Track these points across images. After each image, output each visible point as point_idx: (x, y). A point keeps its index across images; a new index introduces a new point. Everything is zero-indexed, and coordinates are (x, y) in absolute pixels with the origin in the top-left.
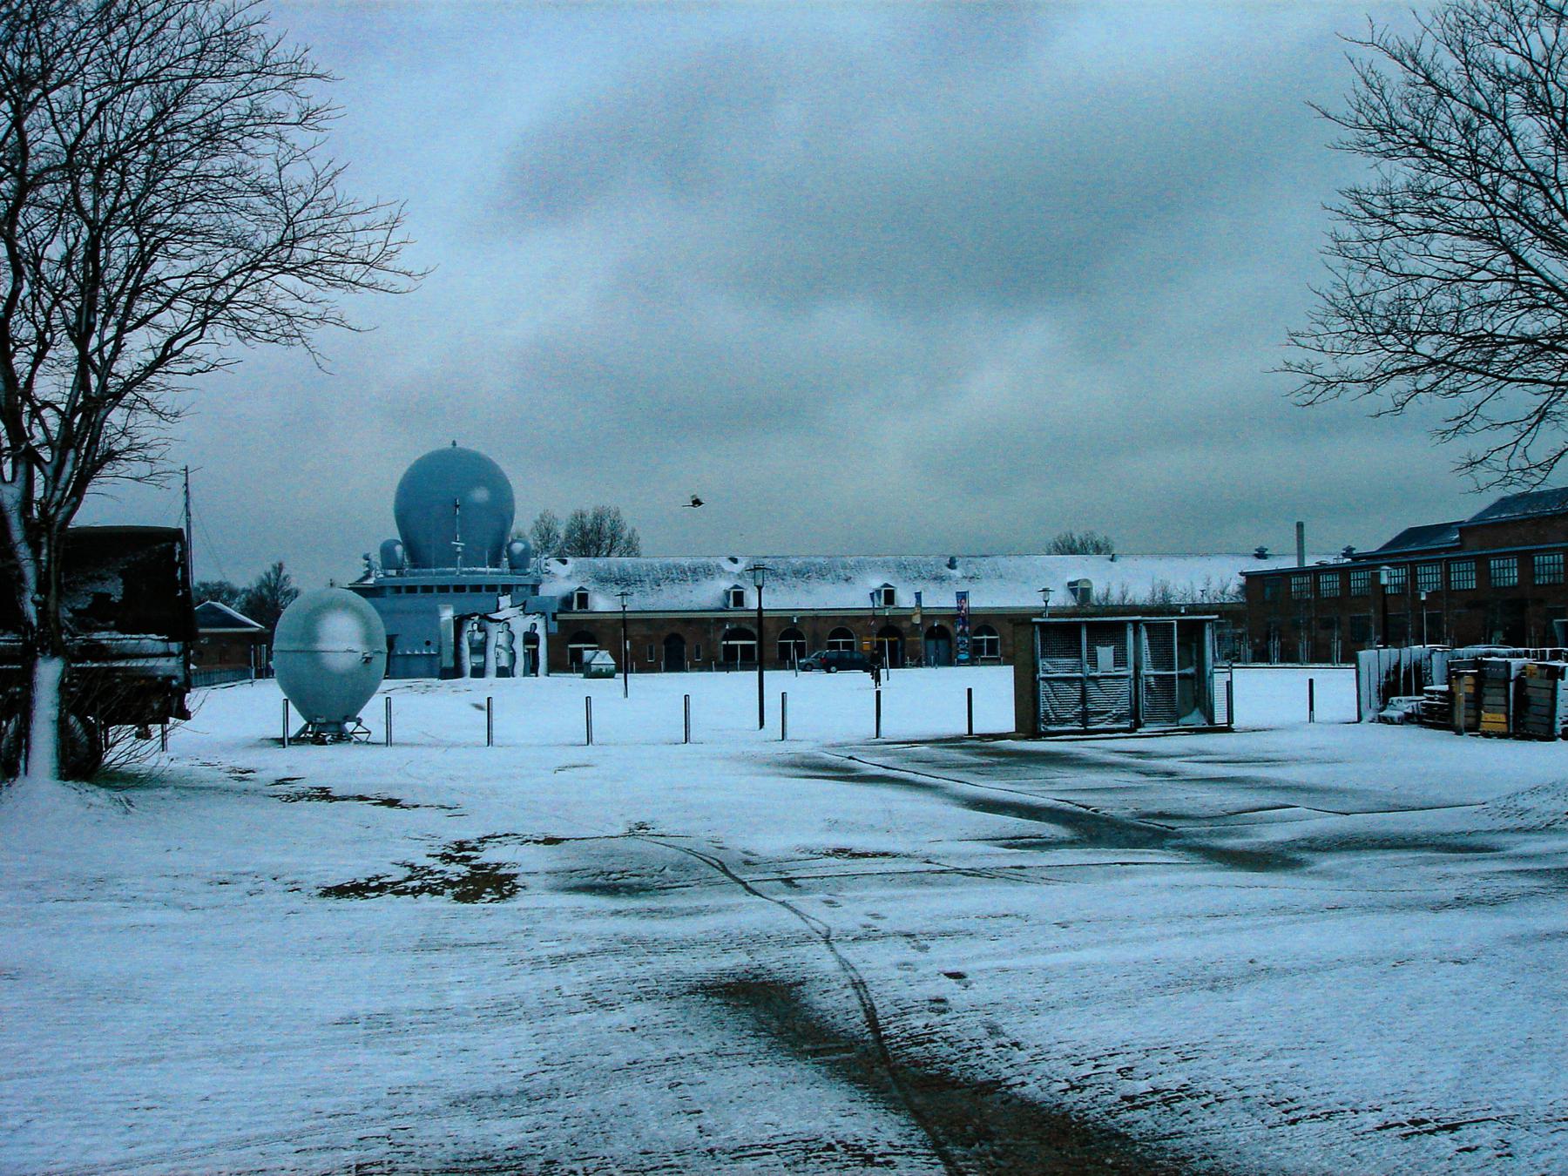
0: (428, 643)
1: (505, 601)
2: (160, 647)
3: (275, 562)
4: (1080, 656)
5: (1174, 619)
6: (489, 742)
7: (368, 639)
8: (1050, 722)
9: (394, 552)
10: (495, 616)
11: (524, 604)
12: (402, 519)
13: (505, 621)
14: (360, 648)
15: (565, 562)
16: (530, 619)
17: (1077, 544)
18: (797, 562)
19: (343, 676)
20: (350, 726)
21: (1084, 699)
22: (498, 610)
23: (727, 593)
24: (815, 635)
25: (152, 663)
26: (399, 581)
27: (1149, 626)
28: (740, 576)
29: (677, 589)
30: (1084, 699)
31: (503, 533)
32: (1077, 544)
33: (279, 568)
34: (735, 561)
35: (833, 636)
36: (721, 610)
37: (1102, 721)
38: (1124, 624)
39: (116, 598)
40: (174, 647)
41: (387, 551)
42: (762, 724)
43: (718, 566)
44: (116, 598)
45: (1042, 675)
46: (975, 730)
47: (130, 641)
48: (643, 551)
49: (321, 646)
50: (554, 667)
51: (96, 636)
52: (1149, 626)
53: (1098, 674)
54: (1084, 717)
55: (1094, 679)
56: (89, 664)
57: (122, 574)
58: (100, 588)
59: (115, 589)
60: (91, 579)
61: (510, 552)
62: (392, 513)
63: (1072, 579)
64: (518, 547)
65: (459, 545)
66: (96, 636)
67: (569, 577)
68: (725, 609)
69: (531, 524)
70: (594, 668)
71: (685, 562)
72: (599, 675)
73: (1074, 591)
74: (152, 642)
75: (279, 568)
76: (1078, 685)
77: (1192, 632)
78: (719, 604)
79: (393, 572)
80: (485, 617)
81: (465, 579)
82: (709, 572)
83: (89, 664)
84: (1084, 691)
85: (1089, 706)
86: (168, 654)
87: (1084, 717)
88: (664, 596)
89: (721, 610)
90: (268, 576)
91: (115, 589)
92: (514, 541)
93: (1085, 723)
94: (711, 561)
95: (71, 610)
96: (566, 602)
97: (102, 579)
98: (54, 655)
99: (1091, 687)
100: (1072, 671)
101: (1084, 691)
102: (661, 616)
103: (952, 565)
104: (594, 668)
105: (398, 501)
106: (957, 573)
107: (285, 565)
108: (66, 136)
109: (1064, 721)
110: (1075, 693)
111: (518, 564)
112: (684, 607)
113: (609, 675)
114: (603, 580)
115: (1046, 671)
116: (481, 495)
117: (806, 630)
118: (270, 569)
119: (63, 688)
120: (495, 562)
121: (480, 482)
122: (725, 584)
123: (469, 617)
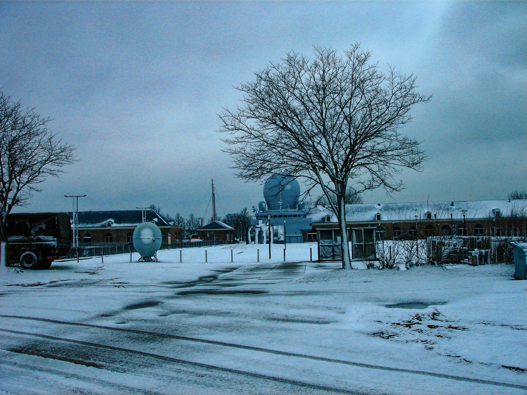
1: (260, 222)
2: (52, 239)
5: (363, 228)
6: (181, 262)
7: (154, 235)
8: (323, 258)
12: (266, 197)
13: (261, 228)
14: (151, 237)
17: (519, 195)
18: (400, 205)
19: (147, 244)
20: (153, 258)
21: (333, 251)
23: (375, 215)
25: (51, 242)
27: (356, 231)
28: (380, 210)
30: (333, 251)
31: (298, 197)
32: (519, 195)
34: (379, 205)
35: (410, 229)
36: (373, 221)
38: (332, 230)
39: (44, 228)
40: (55, 239)
41: (260, 205)
43: (374, 207)
44: (44, 228)
47: (46, 238)
48: (364, 202)
49: (142, 237)
51: (39, 237)
52: (356, 231)
54: (333, 256)
56: (38, 243)
57: (45, 223)
58: (41, 226)
59: (44, 226)
60: (39, 224)
63: (493, 208)
65: (281, 203)
66: (39, 237)
68: (375, 220)
73: (494, 212)
74: (51, 238)
77: (369, 232)
78: (372, 219)
80: (254, 226)
82: (371, 209)
83: (38, 243)
84: (333, 249)
85: (335, 253)
86: (54, 241)
88: (355, 217)
89: (373, 221)
90: (242, 212)
91: (44, 226)
93: (333, 258)
96: (323, 219)
97: (41, 224)
98: (4, 241)
99: (335, 248)
101: (333, 249)
102: (350, 223)
103: (452, 205)
106: (454, 207)
109: (328, 257)
110: (330, 250)
111: (301, 207)
118: (242, 210)
119: (6, 248)
122: (375, 212)
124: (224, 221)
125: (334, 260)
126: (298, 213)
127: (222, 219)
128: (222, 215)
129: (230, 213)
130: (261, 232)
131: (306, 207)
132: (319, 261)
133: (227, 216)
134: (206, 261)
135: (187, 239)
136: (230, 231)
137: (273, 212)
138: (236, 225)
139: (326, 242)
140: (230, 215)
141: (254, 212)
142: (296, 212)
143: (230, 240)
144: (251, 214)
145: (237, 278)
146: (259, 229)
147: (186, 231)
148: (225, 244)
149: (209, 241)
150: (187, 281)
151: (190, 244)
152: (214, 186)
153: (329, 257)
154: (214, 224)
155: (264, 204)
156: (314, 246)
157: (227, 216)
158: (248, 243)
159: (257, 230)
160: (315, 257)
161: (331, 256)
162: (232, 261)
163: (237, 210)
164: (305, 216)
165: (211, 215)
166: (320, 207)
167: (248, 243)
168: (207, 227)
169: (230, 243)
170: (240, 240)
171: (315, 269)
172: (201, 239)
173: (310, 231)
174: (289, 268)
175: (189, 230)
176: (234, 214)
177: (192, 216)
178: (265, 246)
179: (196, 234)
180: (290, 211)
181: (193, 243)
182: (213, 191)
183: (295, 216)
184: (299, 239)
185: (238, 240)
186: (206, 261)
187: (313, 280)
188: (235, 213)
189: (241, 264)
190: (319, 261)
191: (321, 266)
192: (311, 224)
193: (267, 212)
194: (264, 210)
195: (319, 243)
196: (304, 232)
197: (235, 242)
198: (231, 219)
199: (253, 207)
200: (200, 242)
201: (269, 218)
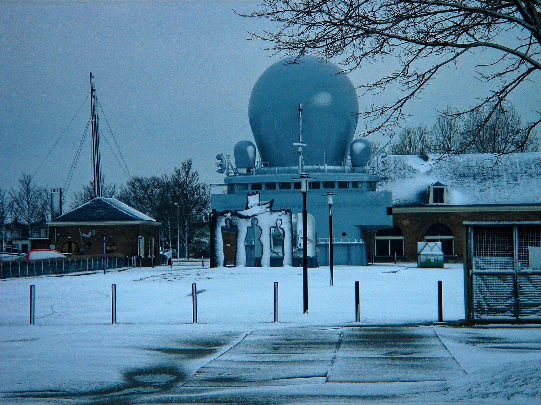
1: (253, 200)
3: (185, 160)
4: (512, 255)
9: (246, 151)
11: (272, 202)
12: (255, 123)
13: (254, 218)
15: (426, 159)
16: (276, 215)
21: (516, 292)
22: (247, 208)
26: (255, 178)
27: (474, 227)
30: (516, 292)
31: (349, 130)
33: (188, 166)
37: (533, 313)
41: (240, 152)
42: (306, 308)
45: (475, 270)
46: (444, 318)
53: (529, 270)
54: (517, 308)
55: (526, 274)
61: (352, 150)
64: (359, 147)
65: (300, 146)
67: (428, 173)
69: (433, 121)
70: (423, 259)
75: (188, 166)
76: (510, 279)
79: (245, 171)
80: (235, 214)
85: (521, 299)
87: (517, 308)
90: (178, 172)
92: (357, 141)
93: (516, 313)
96: (423, 196)
99: (523, 282)
100: (505, 268)
104: (423, 259)
107: (193, 162)
109: (499, 311)
110: (507, 287)
111: (359, 162)
112: (506, 202)
114: (461, 175)
115: (478, 267)
116: (323, 99)
118: (180, 166)
120: (338, 159)
123: (222, 214)
124: (124, 198)
125: (517, 322)
126: (352, 177)
127: (118, 191)
128: (117, 180)
129: (139, 176)
130: (254, 230)
131: (377, 159)
132: (469, 322)
133: (132, 184)
134: (114, 319)
135: (8, 250)
136: (146, 230)
137: (276, 175)
138: (160, 212)
139: (494, 264)
140: (140, 180)
141: (221, 172)
142: (343, 172)
143: (146, 254)
144: (210, 180)
145: (253, 376)
146: (249, 223)
147: (8, 226)
148: (131, 265)
149: (87, 257)
150: (93, 387)
151: (31, 265)
152: (97, 93)
153: (503, 311)
154: (95, 208)
155: (250, 149)
156: (453, 276)
157: (132, 184)
158: (214, 264)
159: (243, 226)
160: (455, 310)
161: (508, 308)
162: (195, 319)
163: (162, 167)
164: (372, 185)
165: (89, 178)
166: (413, 161)
167: (214, 264)
168: (78, 214)
169: (146, 263)
170: (174, 256)
171: (470, 347)
172: (56, 249)
173: (384, 231)
174: (391, 339)
175: (16, 225)
176: (154, 179)
177: (27, 182)
178: (290, 275)
179: (43, 237)
180: (327, 170)
181: (38, 263)
182: (93, 108)
183: (343, 185)
184: (354, 252)
185: (168, 254)
186: (114, 319)
187: (527, 389)
188: (158, 175)
189: (229, 329)
190: (469, 322)
191: (489, 339)
192: (389, 211)
193: (258, 172)
194: (250, 167)
195: (468, 267)
196: (366, 232)
197: (159, 261)
198: (140, 192)
199: (219, 158)
200: (53, 261)
201: (304, 187)
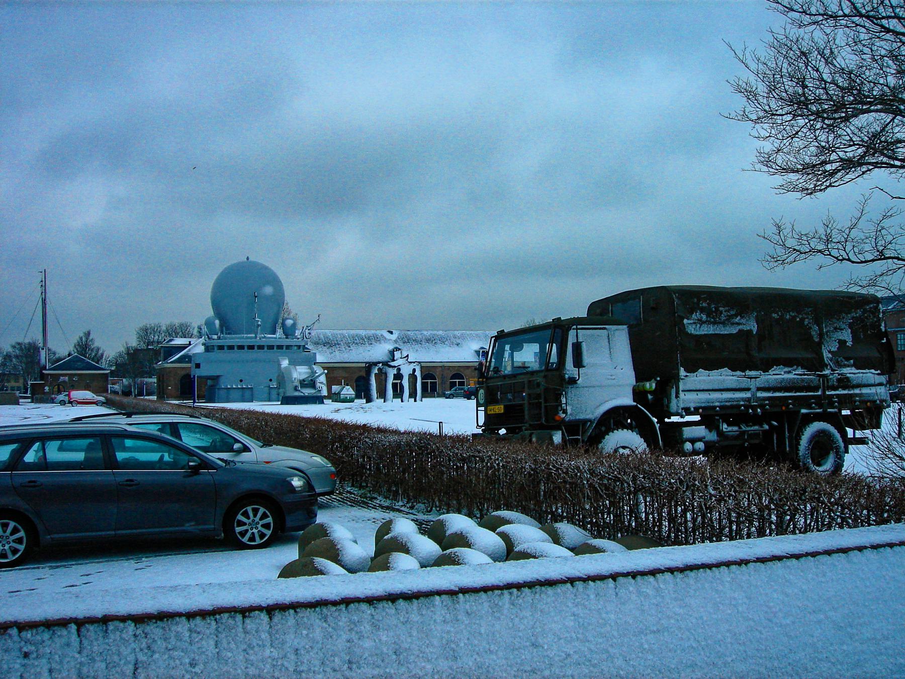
0: (241, 381)
3: (85, 330)
9: (214, 324)
10: (392, 364)
12: (216, 305)
16: (412, 366)
22: (393, 360)
24: (443, 377)
28: (396, 341)
29: (361, 349)
33: (88, 334)
34: (391, 333)
50: (425, 394)
61: (283, 324)
62: (209, 301)
71: (363, 333)
72: (345, 401)
75: (88, 334)
81: (257, 342)
82: (378, 339)
90: (81, 338)
94: (379, 332)
95: (830, 352)
105: (212, 292)
108: (888, 121)
113: (351, 401)
116: (268, 290)
117: (437, 374)
118: (82, 335)
121: (268, 283)
